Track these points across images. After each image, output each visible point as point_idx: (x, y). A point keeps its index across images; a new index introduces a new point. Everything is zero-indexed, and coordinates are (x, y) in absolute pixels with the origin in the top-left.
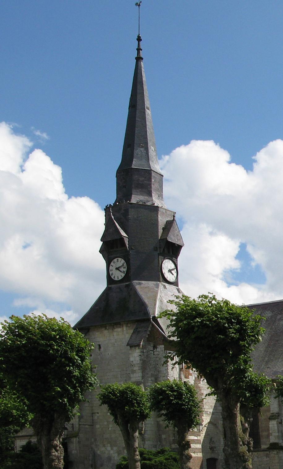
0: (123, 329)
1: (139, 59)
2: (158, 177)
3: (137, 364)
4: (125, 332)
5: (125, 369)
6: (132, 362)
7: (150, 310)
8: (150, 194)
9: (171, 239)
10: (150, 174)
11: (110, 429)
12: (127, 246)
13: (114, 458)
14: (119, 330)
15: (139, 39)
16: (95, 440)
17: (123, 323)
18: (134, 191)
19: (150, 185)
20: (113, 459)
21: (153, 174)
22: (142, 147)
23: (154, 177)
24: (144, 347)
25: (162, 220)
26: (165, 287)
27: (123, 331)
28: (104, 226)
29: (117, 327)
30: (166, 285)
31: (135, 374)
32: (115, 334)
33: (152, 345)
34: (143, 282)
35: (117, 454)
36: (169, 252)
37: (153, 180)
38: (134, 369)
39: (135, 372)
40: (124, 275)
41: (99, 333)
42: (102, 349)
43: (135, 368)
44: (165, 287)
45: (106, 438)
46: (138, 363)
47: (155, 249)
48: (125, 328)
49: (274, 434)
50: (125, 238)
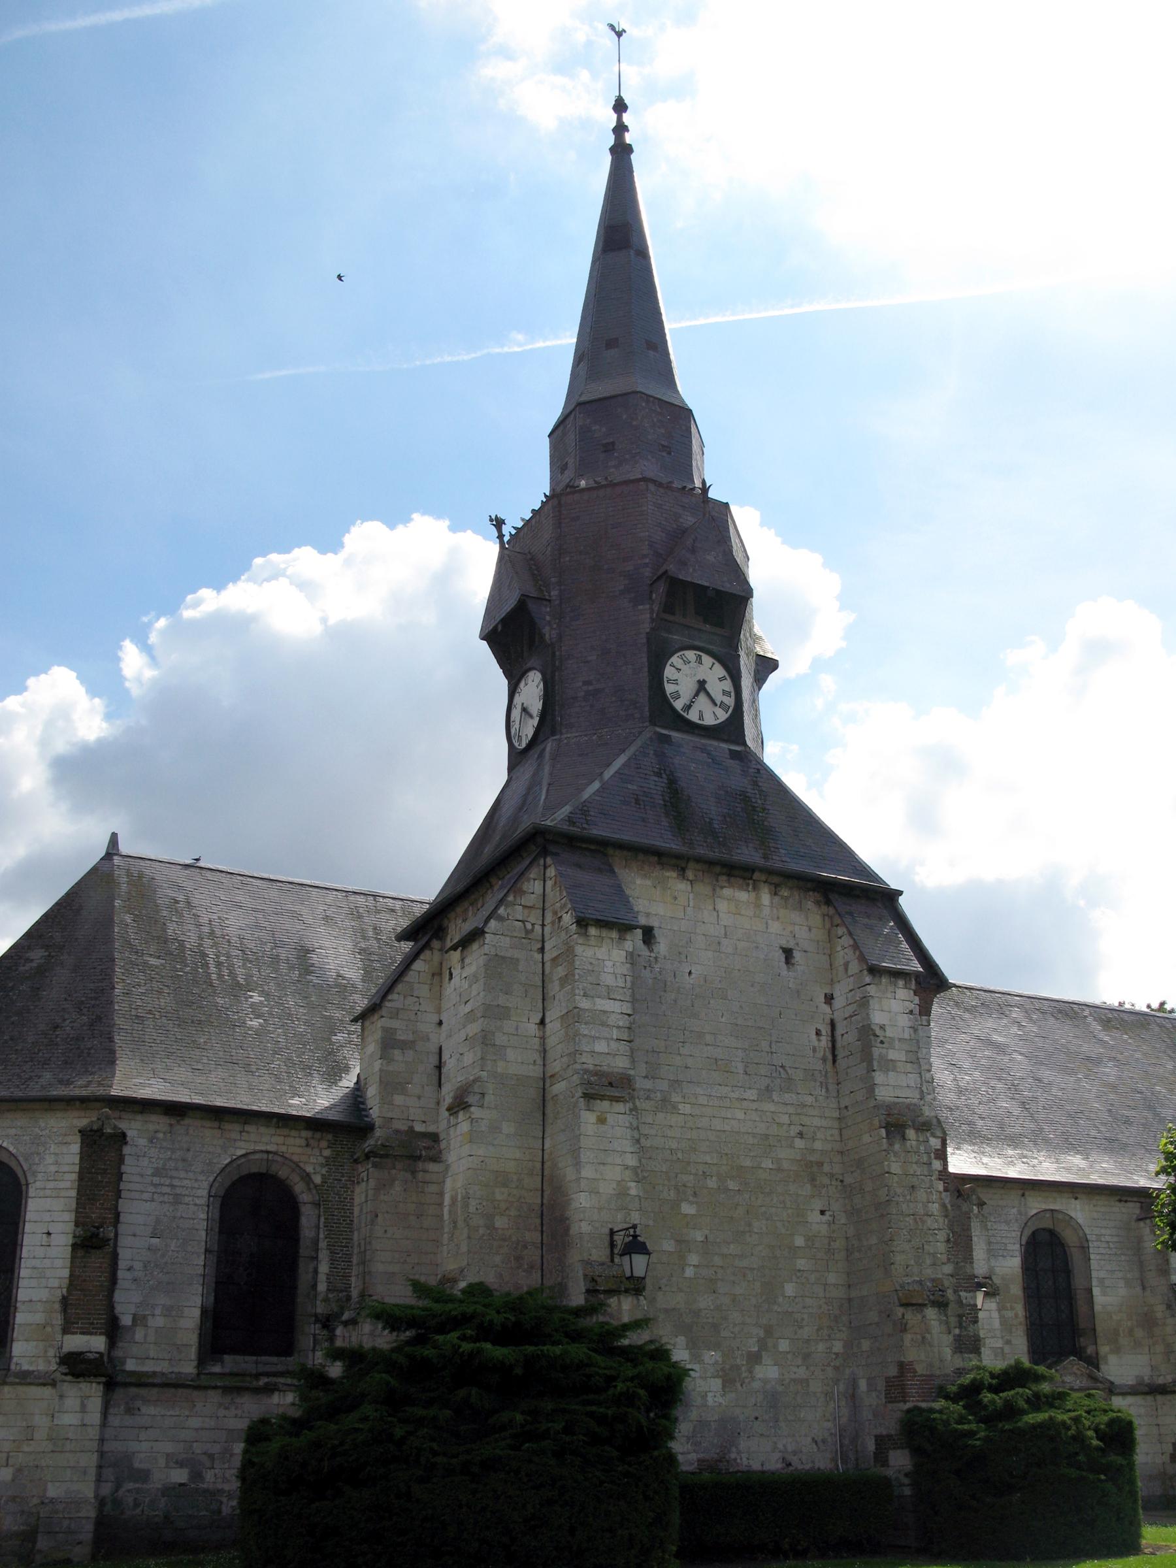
0: (758, 898)
1: (621, 152)
3: (900, 1040)
4: (766, 911)
5: (764, 1045)
6: (882, 1027)
11: (689, 1272)
13: (704, 1396)
14: (743, 896)
15: (620, 106)
17: (763, 878)
20: (699, 1401)
27: (758, 905)
28: (747, 508)
29: (731, 886)
31: (891, 1074)
32: (722, 906)
35: (719, 1381)
38: (890, 1057)
39: (894, 1069)
40: (727, 716)
41: (648, 882)
42: (662, 946)
43: (891, 1051)
45: (666, 1311)
46: (907, 1036)
48: (766, 898)
49: (992, 1340)
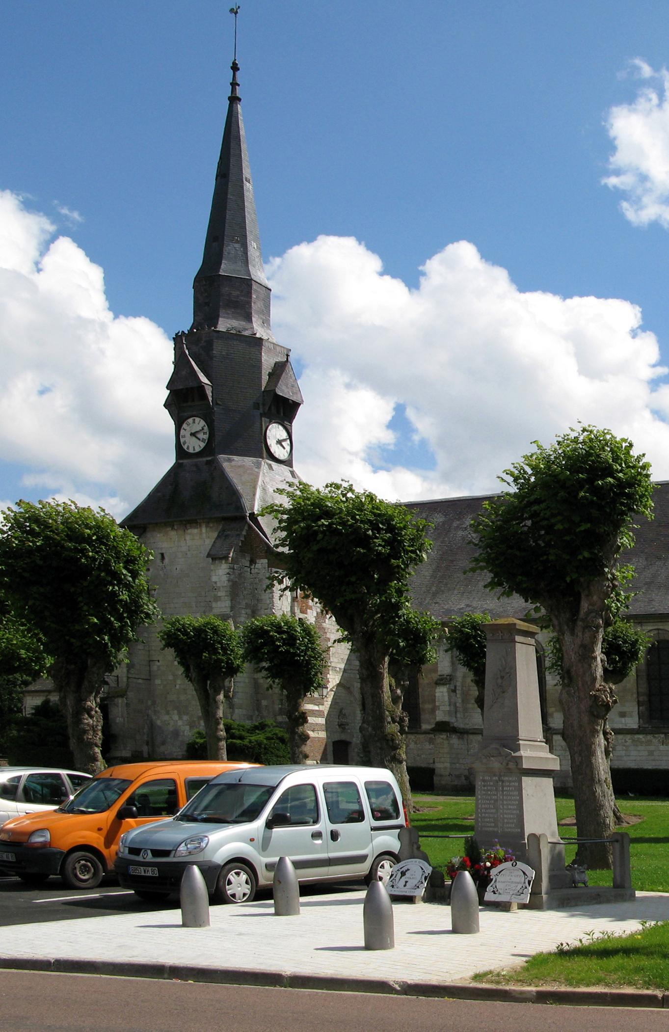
2: (263, 291)
7: (246, 503)
8: (248, 318)
9: (282, 391)
10: (250, 286)
12: (210, 399)
16: (154, 703)
18: (222, 312)
19: (249, 303)
21: (254, 286)
22: (237, 242)
23: (256, 291)
24: (234, 561)
25: (268, 361)
26: (270, 467)
30: (273, 464)
33: (248, 558)
34: (235, 458)
36: (278, 412)
37: (254, 296)
44: (270, 467)
47: (256, 406)
50: (206, 387)
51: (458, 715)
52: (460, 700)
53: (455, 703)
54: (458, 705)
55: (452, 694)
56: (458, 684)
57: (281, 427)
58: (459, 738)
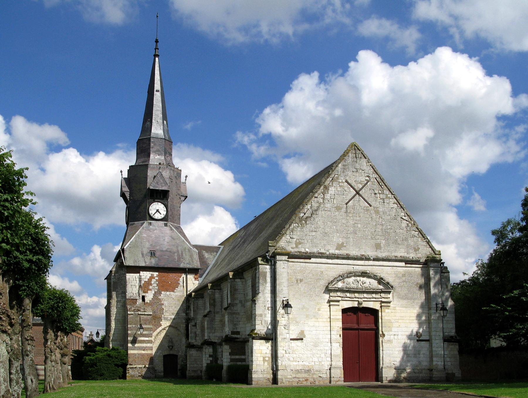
21: (152, 140)
26: (150, 224)
34: (136, 223)
37: (152, 145)
47: (145, 196)
51: (197, 338)
52: (199, 330)
53: (195, 333)
54: (197, 333)
55: (193, 327)
56: (198, 322)
57: (159, 203)
58: (197, 351)
